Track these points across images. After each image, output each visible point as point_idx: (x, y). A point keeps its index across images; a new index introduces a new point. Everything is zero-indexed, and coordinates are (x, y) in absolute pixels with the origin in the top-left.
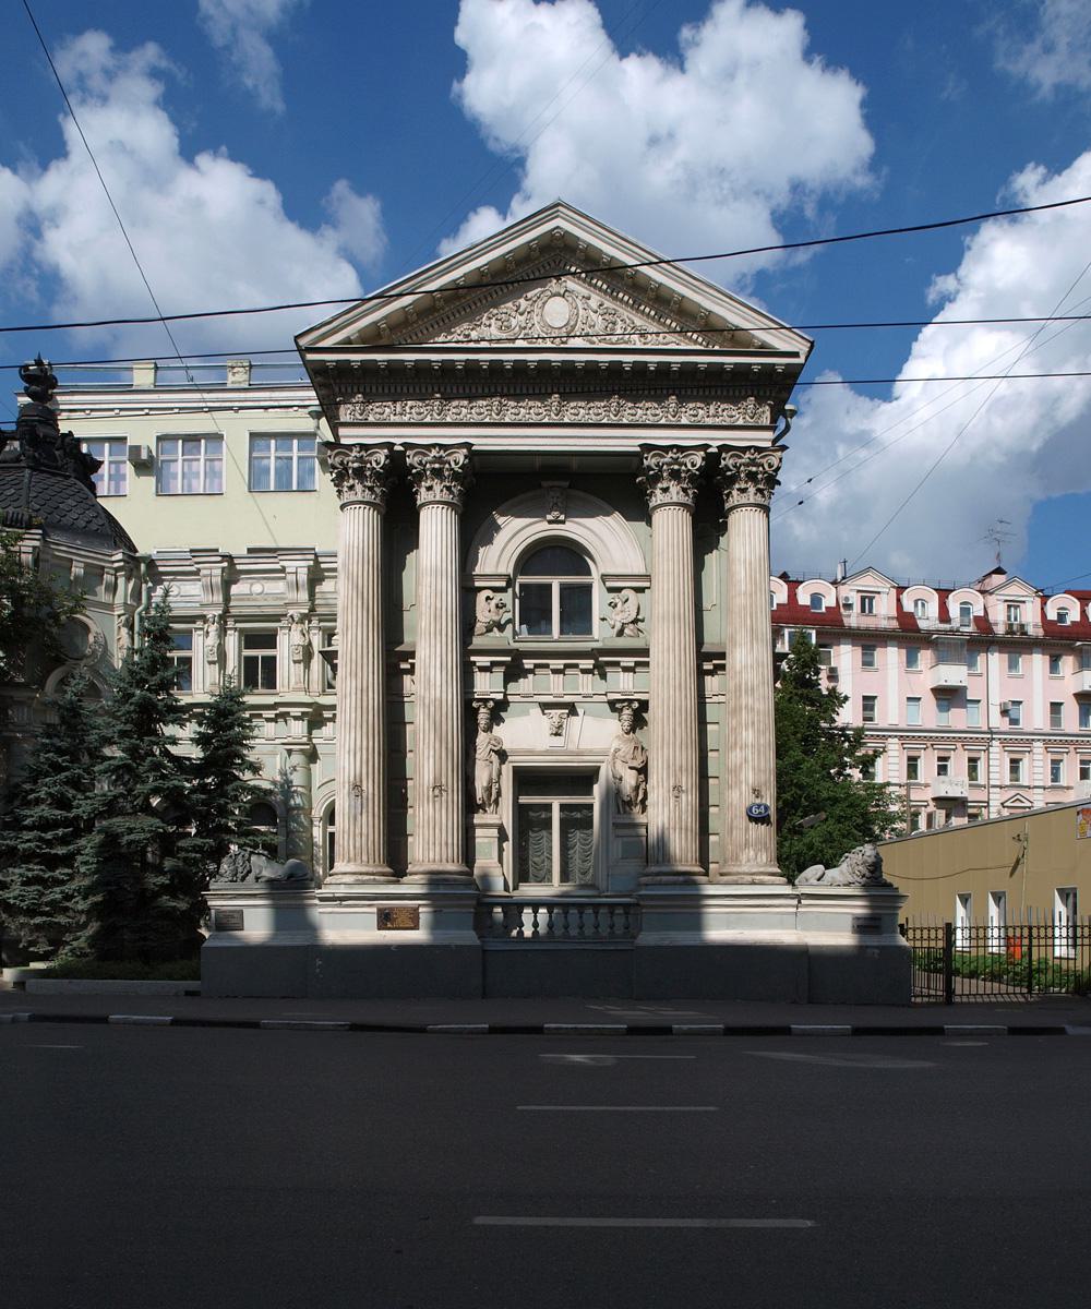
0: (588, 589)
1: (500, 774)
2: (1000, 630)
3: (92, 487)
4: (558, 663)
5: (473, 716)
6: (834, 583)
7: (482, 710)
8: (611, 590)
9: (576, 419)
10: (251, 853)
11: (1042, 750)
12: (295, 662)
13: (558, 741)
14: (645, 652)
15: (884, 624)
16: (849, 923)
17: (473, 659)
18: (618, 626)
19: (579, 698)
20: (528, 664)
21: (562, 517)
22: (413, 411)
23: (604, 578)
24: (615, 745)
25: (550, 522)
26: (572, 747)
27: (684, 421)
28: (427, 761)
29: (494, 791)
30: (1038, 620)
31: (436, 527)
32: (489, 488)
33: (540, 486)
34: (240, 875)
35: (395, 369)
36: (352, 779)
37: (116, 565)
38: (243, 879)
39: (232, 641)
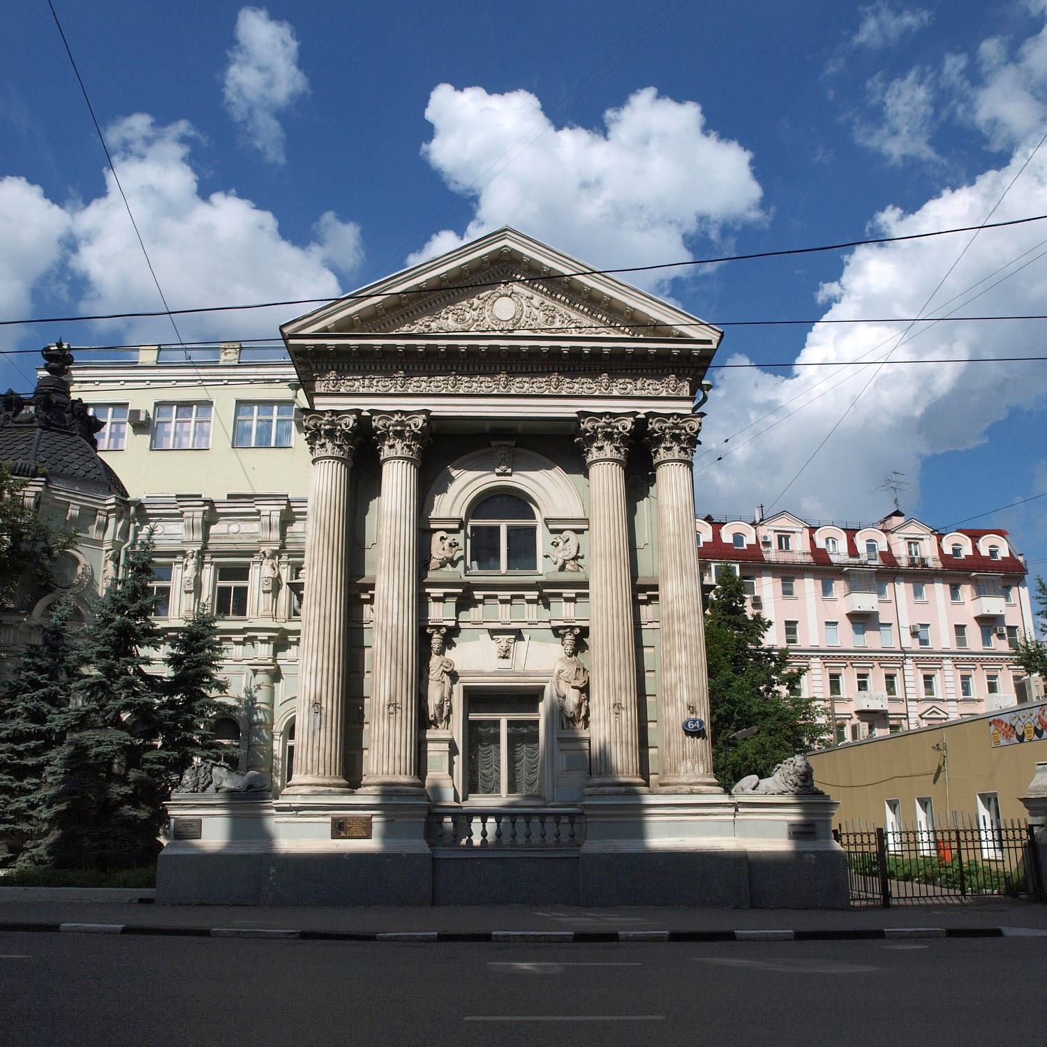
0: (532, 531)
1: (451, 693)
2: (904, 563)
3: (94, 443)
4: (506, 595)
5: (426, 641)
6: (754, 524)
7: (435, 636)
8: (553, 531)
9: (522, 391)
10: (213, 765)
11: (951, 667)
12: (264, 592)
13: (505, 664)
14: (585, 585)
15: (800, 559)
16: (785, 829)
17: (427, 590)
18: (560, 562)
19: (525, 625)
20: (478, 595)
21: (509, 471)
22: (379, 384)
23: (547, 521)
24: (559, 666)
25: (498, 474)
26: (519, 668)
27: (615, 393)
28: (384, 680)
29: (445, 709)
30: (936, 554)
31: (397, 478)
32: (441, 448)
33: (490, 445)
34: (201, 786)
35: (364, 352)
36: (312, 697)
37: (108, 508)
38: (204, 789)
39: (208, 574)
